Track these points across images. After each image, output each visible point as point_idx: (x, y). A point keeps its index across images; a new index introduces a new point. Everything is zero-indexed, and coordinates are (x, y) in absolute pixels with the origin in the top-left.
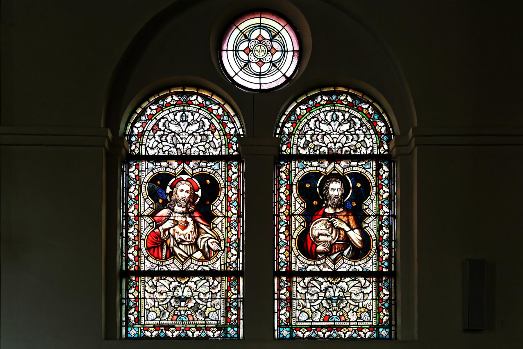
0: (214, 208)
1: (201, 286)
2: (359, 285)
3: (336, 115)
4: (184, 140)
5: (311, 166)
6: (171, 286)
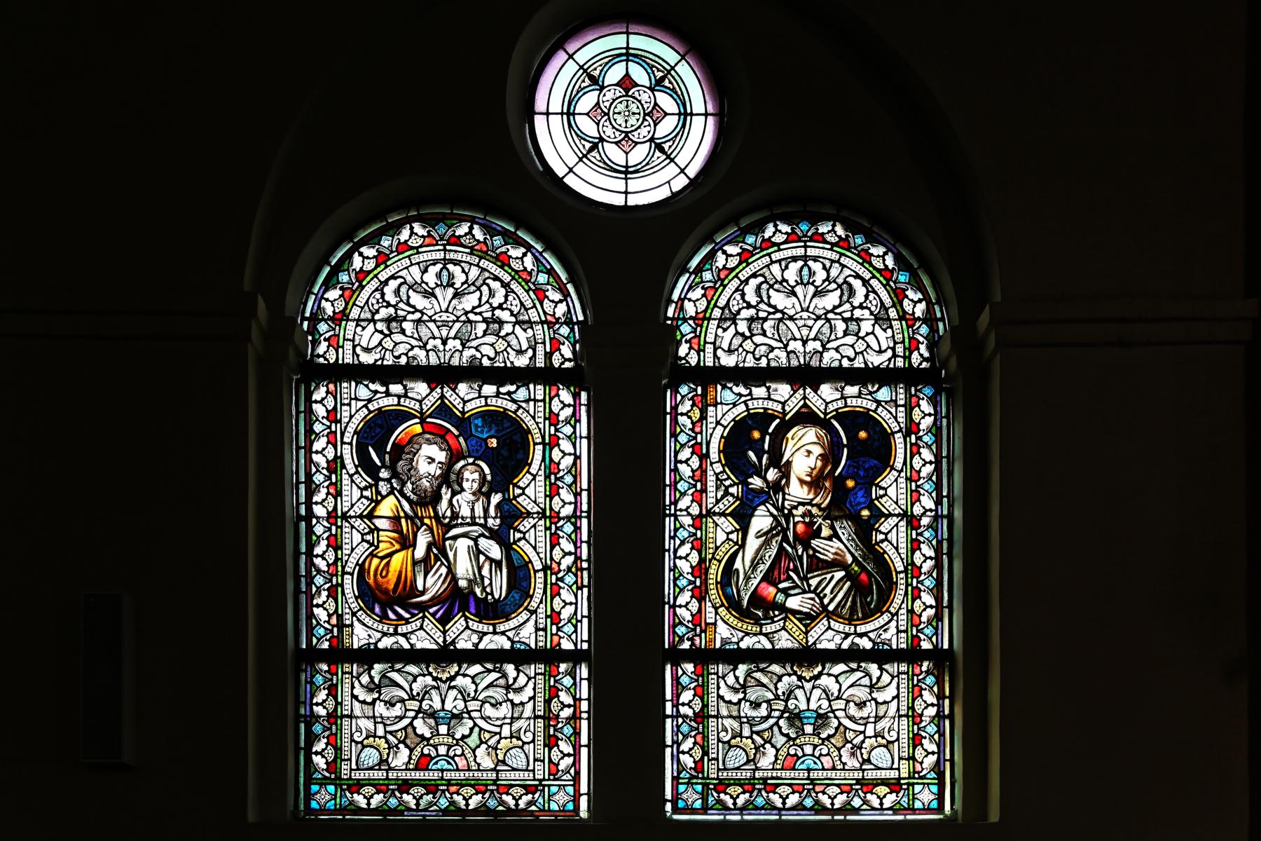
0: (518, 491)
1: (852, 686)
2: (502, 682)
3: (810, 269)
4: (805, 332)
5: (388, 394)
6: (414, 685)
